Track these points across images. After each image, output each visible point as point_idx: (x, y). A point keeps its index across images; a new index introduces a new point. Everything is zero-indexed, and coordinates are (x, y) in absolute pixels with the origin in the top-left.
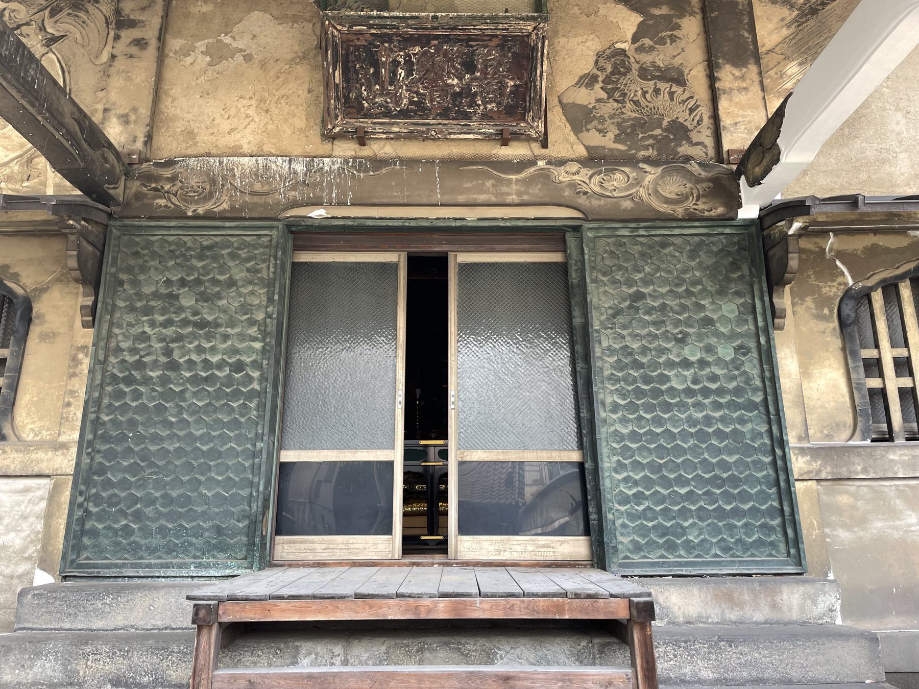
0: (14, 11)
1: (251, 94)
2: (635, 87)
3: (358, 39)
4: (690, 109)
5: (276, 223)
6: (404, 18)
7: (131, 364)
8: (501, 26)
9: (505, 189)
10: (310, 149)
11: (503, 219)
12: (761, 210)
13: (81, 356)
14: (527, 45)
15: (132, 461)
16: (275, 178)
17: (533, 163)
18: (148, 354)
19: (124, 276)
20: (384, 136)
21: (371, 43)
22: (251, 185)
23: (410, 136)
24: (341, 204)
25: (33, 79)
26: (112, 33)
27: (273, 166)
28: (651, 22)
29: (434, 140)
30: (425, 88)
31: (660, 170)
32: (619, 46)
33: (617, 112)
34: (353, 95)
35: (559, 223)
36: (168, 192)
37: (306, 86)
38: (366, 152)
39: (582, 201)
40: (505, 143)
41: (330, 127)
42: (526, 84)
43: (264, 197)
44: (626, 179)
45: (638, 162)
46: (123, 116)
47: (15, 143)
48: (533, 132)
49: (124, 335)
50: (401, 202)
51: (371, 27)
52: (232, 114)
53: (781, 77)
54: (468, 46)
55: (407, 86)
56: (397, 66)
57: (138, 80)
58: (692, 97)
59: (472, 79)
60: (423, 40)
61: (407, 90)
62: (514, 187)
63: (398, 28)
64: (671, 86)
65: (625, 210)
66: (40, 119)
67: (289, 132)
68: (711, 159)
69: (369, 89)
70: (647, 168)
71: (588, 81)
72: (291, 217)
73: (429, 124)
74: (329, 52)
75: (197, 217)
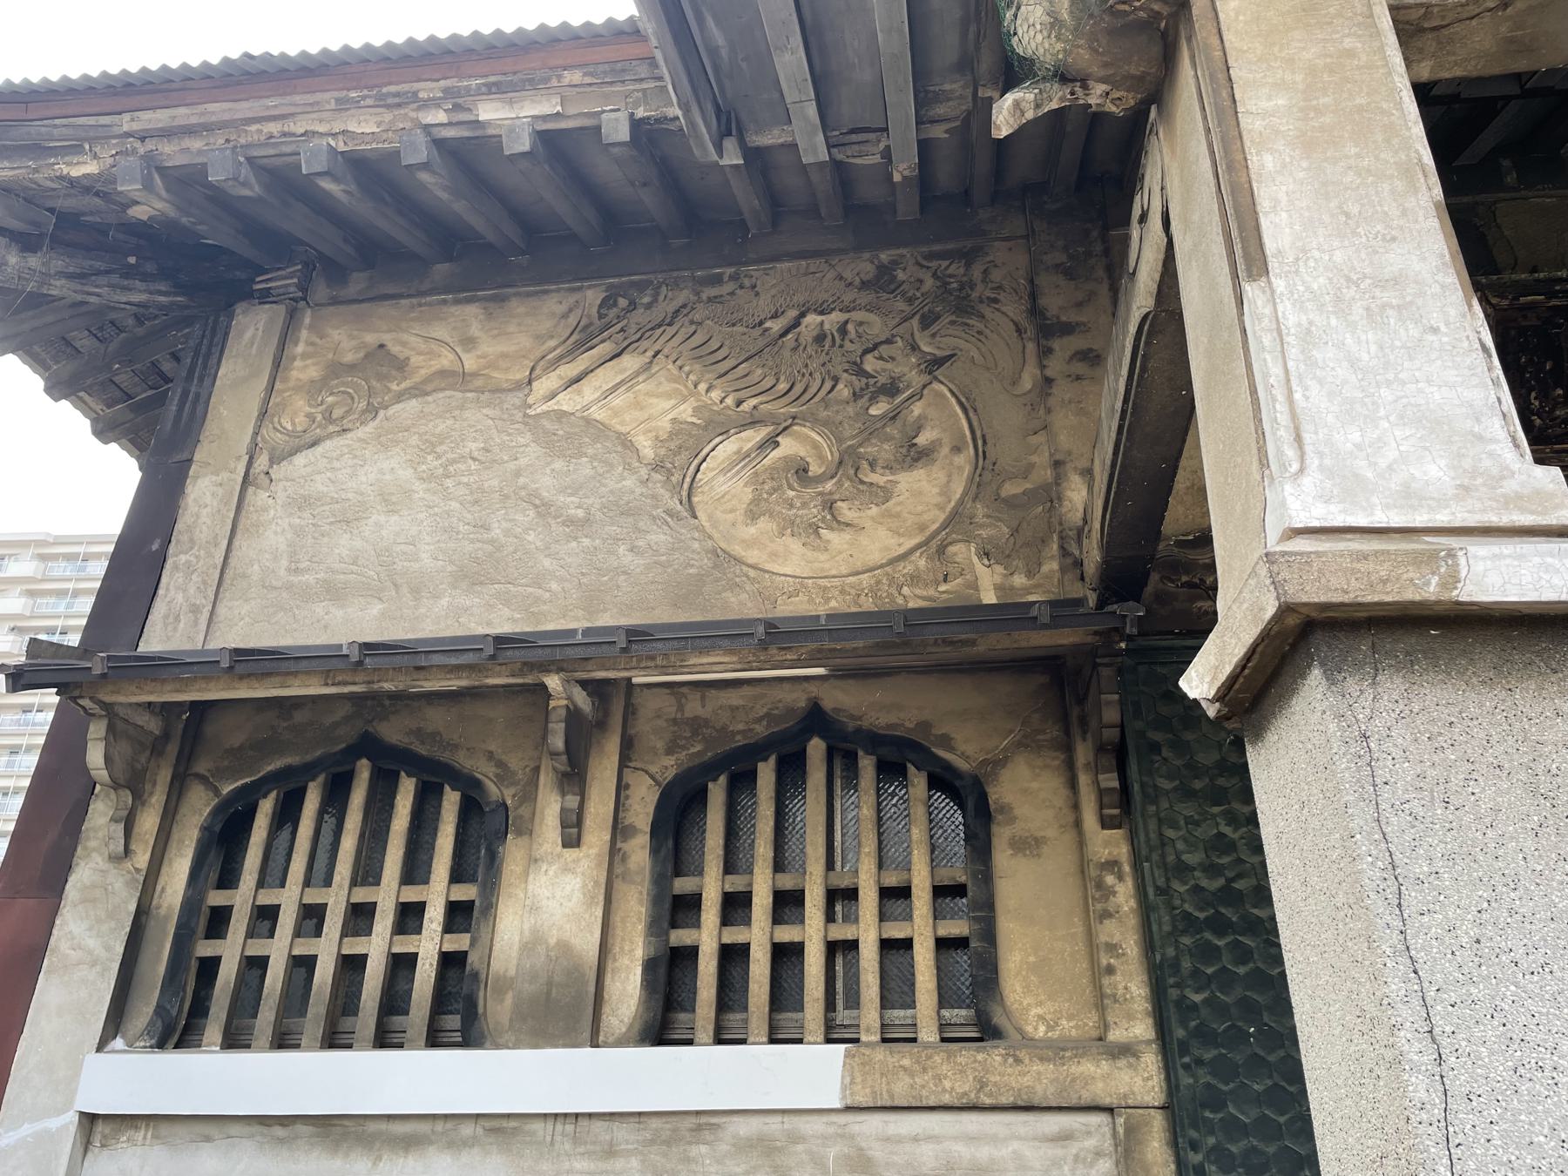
0: (861, 324)
3: (1525, 317)
7: (1214, 894)
13: (1110, 879)
15: (1269, 1082)
18: (1240, 876)
19: (1157, 736)
47: (909, 523)
49: (1185, 840)
51: (1554, 295)
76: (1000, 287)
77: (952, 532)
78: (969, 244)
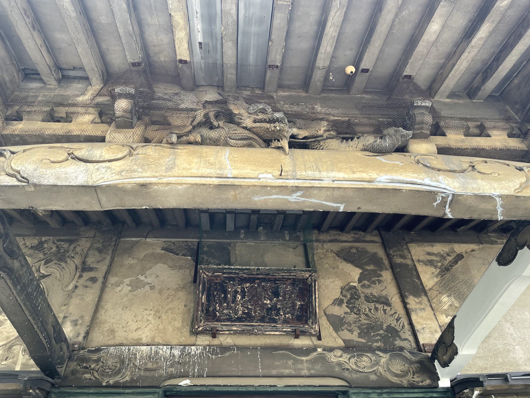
1: (151, 308)
2: (365, 307)
3: (217, 279)
4: (396, 319)
5: (157, 390)
6: (242, 269)
8: (292, 274)
9: (300, 366)
10: (183, 340)
11: (300, 386)
12: (451, 381)
14: (307, 284)
16: (161, 359)
17: (314, 349)
20: (228, 332)
21: (223, 281)
22: (146, 364)
23: (242, 333)
24: (200, 376)
25: (39, 305)
26: (78, 274)
27: (161, 352)
28: (366, 273)
29: (256, 334)
30: (252, 305)
31: (388, 355)
32: (352, 284)
33: (357, 320)
34: (211, 309)
35: (334, 389)
36: (93, 369)
37: (183, 303)
38: (216, 342)
39: (346, 374)
40: (297, 337)
41: (196, 327)
42: (307, 304)
43: (153, 372)
44: (370, 361)
45: (374, 350)
46: (74, 321)
48: (313, 331)
50: (237, 374)
51: (224, 273)
52: (139, 319)
53: (440, 303)
54: (275, 283)
55: (242, 304)
56: (237, 294)
57: (88, 300)
58: (396, 313)
59: (277, 301)
60: (252, 280)
61: (241, 306)
62: (305, 365)
63: (238, 274)
64: (383, 307)
65: (373, 381)
66: (35, 327)
67: (171, 330)
68: (415, 349)
69: (220, 305)
70: (381, 354)
71: (338, 302)
72: (168, 385)
73: (253, 326)
74: (201, 286)
75: (108, 386)
76: (77, 253)
77: (18, 341)
78: (74, 238)
